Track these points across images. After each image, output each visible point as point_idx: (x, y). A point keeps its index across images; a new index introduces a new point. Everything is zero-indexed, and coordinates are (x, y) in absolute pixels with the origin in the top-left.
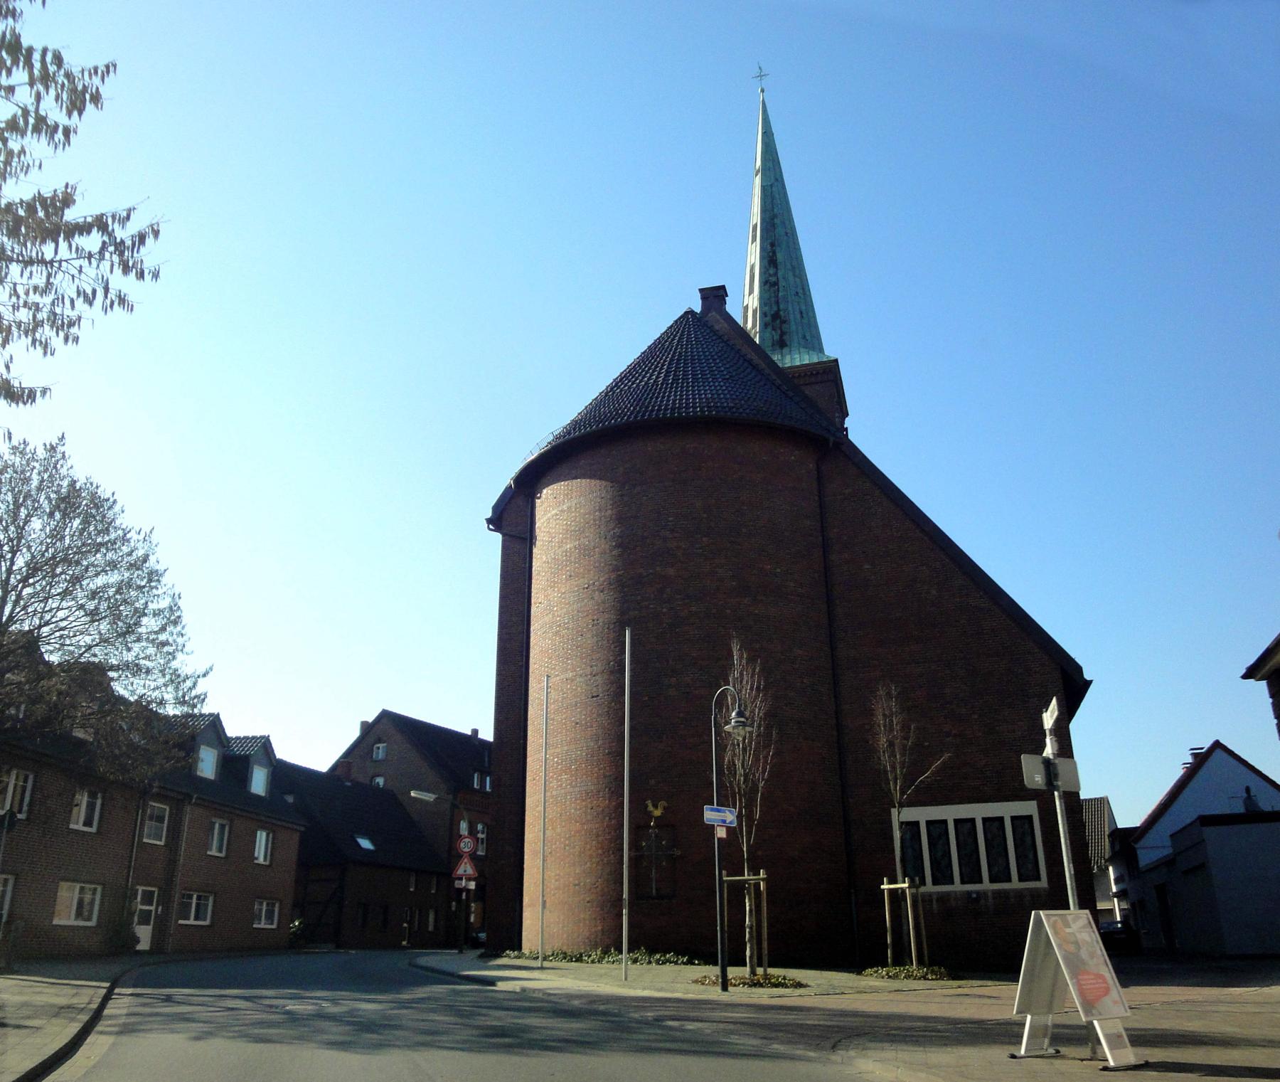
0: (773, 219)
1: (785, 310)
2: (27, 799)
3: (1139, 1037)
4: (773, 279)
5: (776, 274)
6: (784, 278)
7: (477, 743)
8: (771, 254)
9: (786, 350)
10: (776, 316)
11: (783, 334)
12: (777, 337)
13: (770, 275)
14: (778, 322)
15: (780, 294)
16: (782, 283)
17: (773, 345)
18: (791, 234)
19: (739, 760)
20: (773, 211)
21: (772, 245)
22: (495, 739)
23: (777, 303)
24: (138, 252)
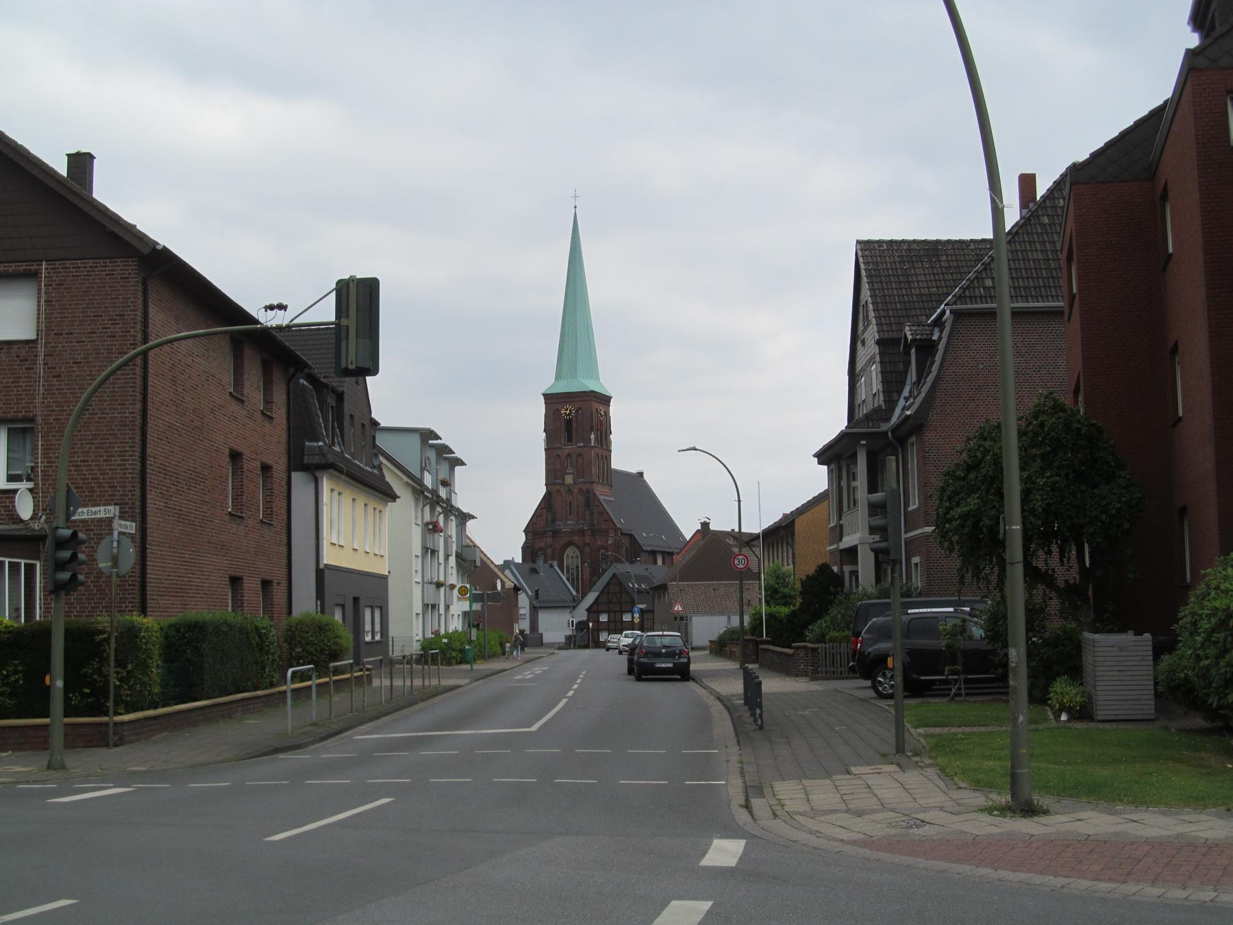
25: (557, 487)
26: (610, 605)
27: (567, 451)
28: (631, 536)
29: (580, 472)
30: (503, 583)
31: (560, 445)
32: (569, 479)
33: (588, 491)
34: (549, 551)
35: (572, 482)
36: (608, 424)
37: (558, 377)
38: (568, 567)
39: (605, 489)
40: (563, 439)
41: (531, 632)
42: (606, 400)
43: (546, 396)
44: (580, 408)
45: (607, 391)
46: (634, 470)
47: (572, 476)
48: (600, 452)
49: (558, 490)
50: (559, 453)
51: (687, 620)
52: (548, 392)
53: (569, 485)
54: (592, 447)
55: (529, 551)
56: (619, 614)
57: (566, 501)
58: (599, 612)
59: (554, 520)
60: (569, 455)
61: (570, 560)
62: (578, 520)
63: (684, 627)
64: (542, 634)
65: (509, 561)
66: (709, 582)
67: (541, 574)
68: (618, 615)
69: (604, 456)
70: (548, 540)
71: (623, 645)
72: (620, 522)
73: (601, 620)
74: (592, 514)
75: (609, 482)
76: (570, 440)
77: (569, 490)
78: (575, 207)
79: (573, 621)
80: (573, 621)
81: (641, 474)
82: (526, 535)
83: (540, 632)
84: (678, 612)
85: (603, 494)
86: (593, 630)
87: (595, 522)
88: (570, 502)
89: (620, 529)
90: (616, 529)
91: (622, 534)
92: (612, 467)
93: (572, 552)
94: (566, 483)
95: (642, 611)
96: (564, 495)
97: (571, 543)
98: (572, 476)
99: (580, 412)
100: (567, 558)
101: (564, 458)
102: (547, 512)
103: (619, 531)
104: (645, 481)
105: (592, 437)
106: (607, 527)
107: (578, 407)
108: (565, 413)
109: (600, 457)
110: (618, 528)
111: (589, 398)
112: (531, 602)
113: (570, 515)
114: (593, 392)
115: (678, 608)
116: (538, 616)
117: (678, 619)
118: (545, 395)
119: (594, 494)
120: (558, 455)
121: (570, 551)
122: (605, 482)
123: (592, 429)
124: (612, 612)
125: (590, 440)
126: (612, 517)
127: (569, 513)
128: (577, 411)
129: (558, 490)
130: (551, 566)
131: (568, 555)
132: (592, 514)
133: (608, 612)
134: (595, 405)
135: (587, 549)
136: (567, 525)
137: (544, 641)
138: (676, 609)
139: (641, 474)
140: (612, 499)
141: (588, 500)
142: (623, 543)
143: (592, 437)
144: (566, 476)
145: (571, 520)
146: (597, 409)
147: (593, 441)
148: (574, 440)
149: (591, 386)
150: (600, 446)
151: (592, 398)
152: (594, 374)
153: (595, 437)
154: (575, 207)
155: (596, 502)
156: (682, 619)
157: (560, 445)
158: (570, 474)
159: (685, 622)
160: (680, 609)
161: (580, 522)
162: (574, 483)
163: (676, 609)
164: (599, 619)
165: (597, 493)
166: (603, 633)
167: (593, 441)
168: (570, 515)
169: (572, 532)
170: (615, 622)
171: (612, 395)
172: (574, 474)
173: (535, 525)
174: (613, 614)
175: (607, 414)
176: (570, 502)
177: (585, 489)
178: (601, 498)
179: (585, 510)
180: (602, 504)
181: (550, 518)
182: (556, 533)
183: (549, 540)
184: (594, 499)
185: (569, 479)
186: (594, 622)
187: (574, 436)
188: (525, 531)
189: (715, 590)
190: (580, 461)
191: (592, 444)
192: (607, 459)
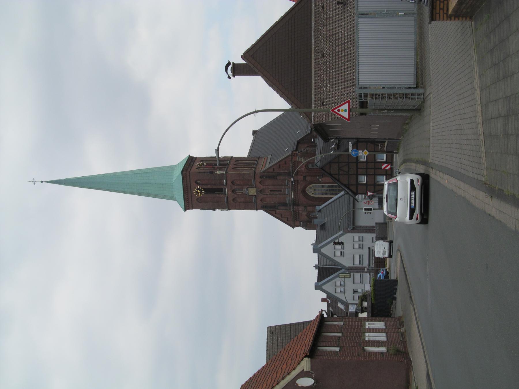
25: (259, 201)
26: (350, 173)
27: (230, 193)
28: (299, 142)
29: (247, 183)
30: (303, 374)
31: (225, 198)
32: (252, 192)
33: (262, 177)
34: (309, 209)
35: (255, 189)
36: (211, 159)
37: (172, 198)
38: (322, 194)
39: (262, 162)
40: (221, 196)
41: (374, 233)
42: (191, 160)
43: (186, 209)
44: (196, 182)
45: (182, 162)
46: (251, 138)
47: (250, 189)
48: (231, 166)
49: (261, 200)
50: (232, 199)
51: (366, 96)
52: (183, 206)
53: (257, 191)
54: (226, 173)
55: (308, 225)
56: (359, 164)
57: (270, 194)
58: (357, 184)
59: (285, 204)
60: (233, 191)
61: (317, 192)
62: (285, 185)
63: (378, 101)
64: (376, 223)
65: (314, 249)
66: (313, 64)
67: (326, 221)
68: (360, 165)
69: (235, 163)
70: (300, 210)
71: (411, 217)
72: (287, 151)
73: (365, 182)
74: (280, 174)
75: (256, 159)
76: (221, 190)
77: (261, 191)
78: (42, 182)
79: (365, 209)
80: (365, 209)
81: (255, 132)
82: (296, 226)
83: (375, 225)
84: (350, 110)
85: (264, 166)
86: (374, 192)
87: (287, 171)
88: (270, 191)
89: (293, 151)
90: (293, 155)
91: (296, 150)
92: (246, 156)
93: (311, 190)
94: (255, 194)
95: (356, 147)
96: (265, 196)
97: (304, 191)
98: (250, 189)
99: (199, 182)
100: (315, 194)
101: (236, 196)
102: (278, 209)
103: (295, 152)
104: (260, 130)
105: (218, 172)
106: (291, 162)
107: (194, 184)
108: (201, 193)
109: (235, 166)
110: (292, 153)
111: (188, 175)
112: (349, 232)
113: (281, 191)
114: (182, 171)
115: (344, 111)
116: (361, 226)
117: (364, 110)
118: (186, 210)
119: (264, 172)
120: (233, 200)
121: (310, 191)
122: (256, 162)
123: (212, 173)
124: (357, 172)
125: (221, 174)
126: (282, 158)
127: (279, 192)
128: (197, 184)
129: (261, 200)
130: (320, 211)
131: (313, 194)
132: (280, 174)
133: (357, 175)
134: (194, 169)
135: (308, 178)
136: (289, 196)
137: (382, 221)
138: (345, 115)
139: (255, 132)
140: (269, 157)
141: (269, 177)
142: (304, 150)
143: (218, 172)
144: (250, 194)
145: (285, 191)
146: (197, 168)
147: (222, 172)
148: (221, 187)
149: (178, 174)
150: (227, 166)
151: (188, 173)
152: (173, 168)
153: (219, 170)
154: (42, 182)
155: (271, 170)
156: (363, 105)
157: (225, 198)
158: (248, 190)
159: (369, 98)
160: (346, 106)
161: (287, 184)
162: (255, 187)
163: (345, 115)
164: (363, 162)
165: (263, 169)
166: (378, 180)
167: (222, 172)
168: (281, 191)
169: (294, 189)
170: (367, 169)
171: (188, 155)
172: (248, 188)
173: (289, 219)
174: (360, 171)
175: (202, 160)
176: (270, 191)
177: (261, 179)
178: (268, 166)
179: (277, 179)
180: (272, 166)
181: (282, 208)
182: (295, 204)
183: (301, 208)
184: (268, 172)
185: (252, 192)
186: (367, 190)
187: (218, 187)
188: (293, 227)
189: (323, 56)
190: (238, 182)
191: (224, 172)
192: (238, 161)
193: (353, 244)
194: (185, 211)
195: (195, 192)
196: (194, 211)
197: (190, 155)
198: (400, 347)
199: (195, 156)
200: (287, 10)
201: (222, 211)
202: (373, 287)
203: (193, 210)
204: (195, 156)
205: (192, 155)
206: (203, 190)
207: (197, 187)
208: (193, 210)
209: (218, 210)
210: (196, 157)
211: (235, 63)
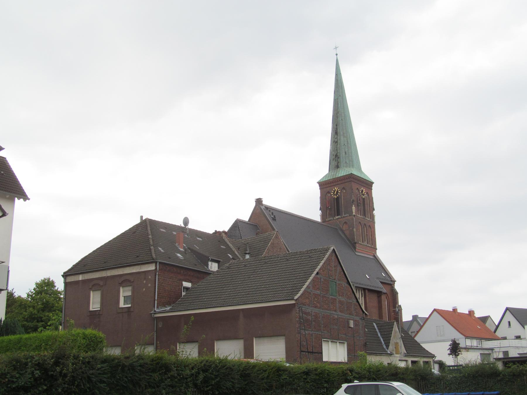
0: (337, 114)
1: (339, 153)
2: (361, 249)
3: (334, 163)
4: (336, 140)
5: (337, 138)
6: (339, 139)
7: (500, 366)
8: (336, 129)
9: (339, 169)
10: (336, 156)
11: (338, 162)
12: (336, 164)
13: (335, 139)
14: (337, 158)
15: (338, 146)
16: (339, 142)
17: (335, 167)
18: (339, 66)
19: (104, 386)
20: (337, 110)
21: (337, 125)
22: (323, 216)
23: (337, 150)
24: (386, 296)
45: (367, 177)
78: (337, 55)
134: (355, 186)
154: (337, 55)
171: (373, 181)
193: (415, 332)
194: (317, 183)
195: (335, 189)
196: (319, 191)
197: (373, 183)
198: (321, 352)
199: (373, 189)
200: (402, 301)
201: (319, 216)
202: (156, 357)
203: (320, 190)
204: (373, 188)
205: (374, 185)
206: (337, 196)
207: (339, 191)
208: (319, 190)
209: (320, 213)
210: (372, 189)
211: (373, 184)
